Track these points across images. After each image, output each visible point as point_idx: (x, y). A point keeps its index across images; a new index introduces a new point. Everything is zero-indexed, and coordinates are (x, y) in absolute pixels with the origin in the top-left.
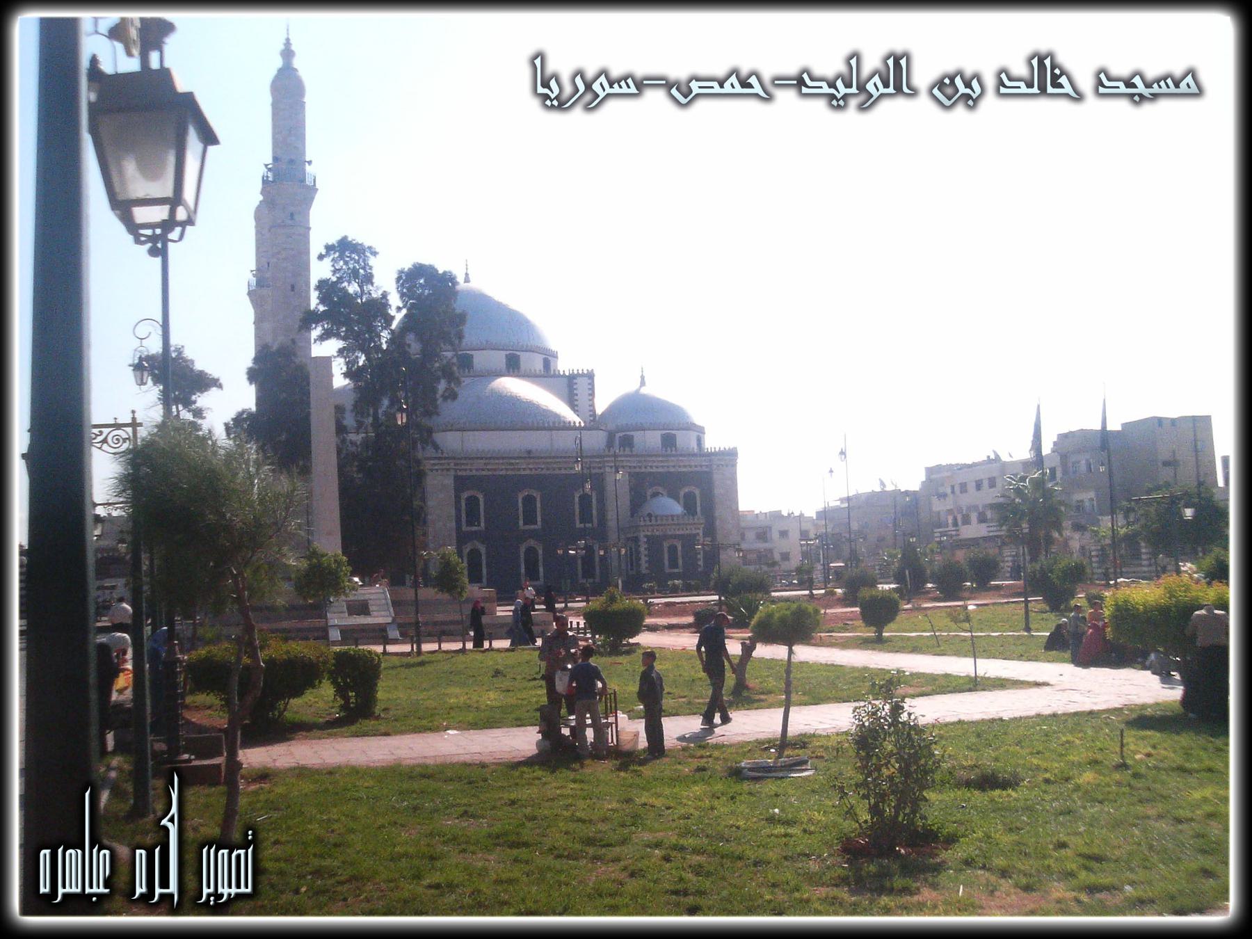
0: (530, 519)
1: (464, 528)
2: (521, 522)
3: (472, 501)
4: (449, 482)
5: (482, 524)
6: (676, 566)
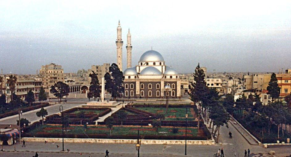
3: (142, 85)
4: (139, 82)
5: (151, 88)
6: (151, 95)
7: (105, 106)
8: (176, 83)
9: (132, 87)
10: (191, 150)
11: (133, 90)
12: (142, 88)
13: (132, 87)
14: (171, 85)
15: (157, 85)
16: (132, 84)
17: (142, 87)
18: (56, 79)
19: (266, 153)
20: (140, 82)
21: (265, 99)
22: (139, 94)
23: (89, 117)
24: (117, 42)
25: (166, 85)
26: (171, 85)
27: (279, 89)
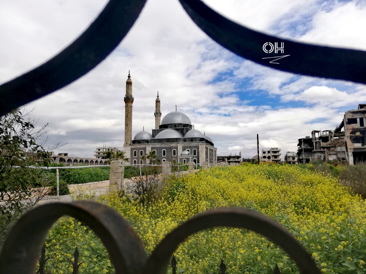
0: (164, 154)
15: (163, 150)
20: (152, 147)
26: (191, 150)
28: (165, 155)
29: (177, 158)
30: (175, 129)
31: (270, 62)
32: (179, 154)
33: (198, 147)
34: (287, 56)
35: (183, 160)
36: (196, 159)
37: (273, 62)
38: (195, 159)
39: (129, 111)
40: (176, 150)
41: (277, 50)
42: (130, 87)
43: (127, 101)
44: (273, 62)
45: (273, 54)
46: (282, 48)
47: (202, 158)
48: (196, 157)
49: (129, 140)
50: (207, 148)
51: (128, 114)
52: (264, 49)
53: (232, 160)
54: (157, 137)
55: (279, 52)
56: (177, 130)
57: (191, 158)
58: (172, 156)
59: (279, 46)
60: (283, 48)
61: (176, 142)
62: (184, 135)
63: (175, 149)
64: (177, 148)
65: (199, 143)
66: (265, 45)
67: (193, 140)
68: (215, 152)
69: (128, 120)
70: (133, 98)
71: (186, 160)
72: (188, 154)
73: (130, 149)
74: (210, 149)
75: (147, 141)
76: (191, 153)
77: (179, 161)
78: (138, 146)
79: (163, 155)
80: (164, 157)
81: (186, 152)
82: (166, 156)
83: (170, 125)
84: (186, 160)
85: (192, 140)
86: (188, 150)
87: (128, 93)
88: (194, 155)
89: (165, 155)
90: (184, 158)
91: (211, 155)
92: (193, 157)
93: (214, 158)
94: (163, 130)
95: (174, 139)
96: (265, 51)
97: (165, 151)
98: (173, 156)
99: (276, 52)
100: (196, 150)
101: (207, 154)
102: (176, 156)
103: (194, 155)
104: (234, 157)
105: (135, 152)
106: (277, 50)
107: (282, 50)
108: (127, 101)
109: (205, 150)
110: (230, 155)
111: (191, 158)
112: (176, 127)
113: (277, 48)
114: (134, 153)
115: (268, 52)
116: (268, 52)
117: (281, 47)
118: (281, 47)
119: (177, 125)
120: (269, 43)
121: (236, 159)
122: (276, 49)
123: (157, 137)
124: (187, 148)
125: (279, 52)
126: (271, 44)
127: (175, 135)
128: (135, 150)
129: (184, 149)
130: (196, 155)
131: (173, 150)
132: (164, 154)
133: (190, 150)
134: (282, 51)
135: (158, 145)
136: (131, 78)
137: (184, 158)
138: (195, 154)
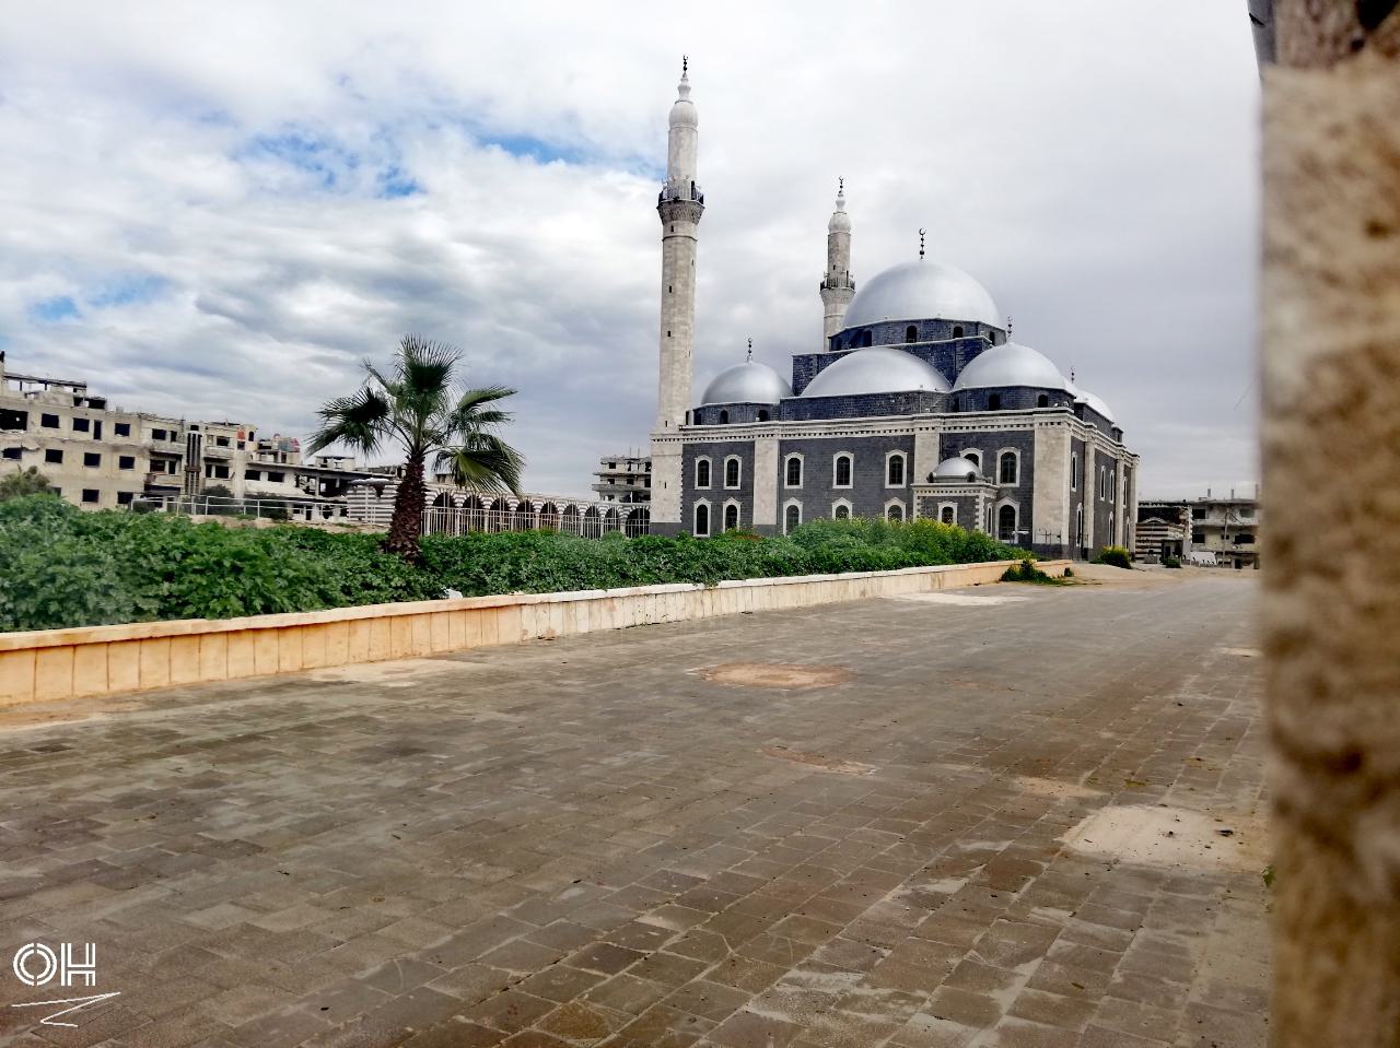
0: (844, 479)
1: (786, 486)
2: (725, 484)
4: (776, 447)
5: (1018, 480)
7: (481, 653)
8: (1032, 443)
9: (732, 480)
10: (427, 918)
11: (708, 495)
12: (790, 483)
13: (732, 480)
14: (990, 458)
15: (836, 458)
16: (734, 457)
17: (794, 479)
18: (23, 425)
19: (1201, 995)
20: (781, 443)
21: (123, 422)
22: (772, 521)
23: (136, 695)
24: (822, 286)
25: (959, 455)
26: (990, 458)
27: (376, 419)
28: (847, 483)
29: (907, 496)
30: (907, 349)
31: (42, 1021)
32: (920, 478)
33: (1025, 440)
34: (108, 995)
35: (941, 506)
36: (1016, 507)
37: (53, 1020)
38: (1007, 502)
39: (681, 263)
40: (904, 456)
41: (70, 973)
42: (685, 142)
43: (671, 213)
44: (53, 1020)
45: (54, 990)
46: (87, 965)
47: (1046, 496)
48: (1014, 491)
49: (678, 408)
50: (1079, 447)
51: (673, 278)
52: (22, 973)
53: (1213, 519)
54: (818, 388)
55: (79, 978)
56: (917, 352)
57: (983, 495)
58: (882, 489)
59: (78, 956)
60: (93, 965)
61: (905, 412)
62: (952, 378)
63: (901, 448)
64: (908, 443)
65: (1038, 419)
66: (23, 953)
67: (1003, 401)
68: (1128, 472)
69: (673, 306)
70: (701, 200)
71: (954, 506)
72: (971, 477)
73: (680, 451)
74: (1098, 453)
75: (764, 412)
76: (989, 471)
77: (916, 513)
78: (716, 434)
79: (839, 482)
80: (841, 493)
81: (961, 467)
82: (850, 486)
83: (882, 331)
84: (954, 506)
85: (995, 399)
86: (973, 458)
87: (678, 170)
88: (1004, 480)
89: (847, 483)
90: (943, 499)
91: (1106, 486)
92: (1000, 490)
93: (1121, 507)
94: (846, 353)
95: (897, 395)
96: (23, 975)
97: (847, 460)
98: (888, 486)
99: (67, 980)
100: (1018, 454)
101: (1078, 478)
102: (903, 486)
103: (1004, 480)
104: (1225, 507)
105: (704, 464)
106: (70, 973)
107: (87, 973)
108: (671, 213)
109: (1067, 456)
110: (1204, 495)
111: (983, 495)
112: (917, 337)
113: (70, 965)
114: (700, 470)
115: (36, 981)
116: (36, 981)
117: (85, 963)
118: (85, 963)
119: (919, 329)
120: (39, 945)
121: (1238, 516)
122: (67, 969)
123: (810, 392)
124: (966, 445)
125: (79, 978)
126: (44, 950)
127: (913, 376)
128: (702, 453)
129: (950, 447)
130: (1013, 481)
131: (889, 456)
132: (844, 479)
133: (979, 453)
134: (91, 977)
135: (816, 430)
136: (692, 96)
137: (943, 499)
138: (1008, 476)
